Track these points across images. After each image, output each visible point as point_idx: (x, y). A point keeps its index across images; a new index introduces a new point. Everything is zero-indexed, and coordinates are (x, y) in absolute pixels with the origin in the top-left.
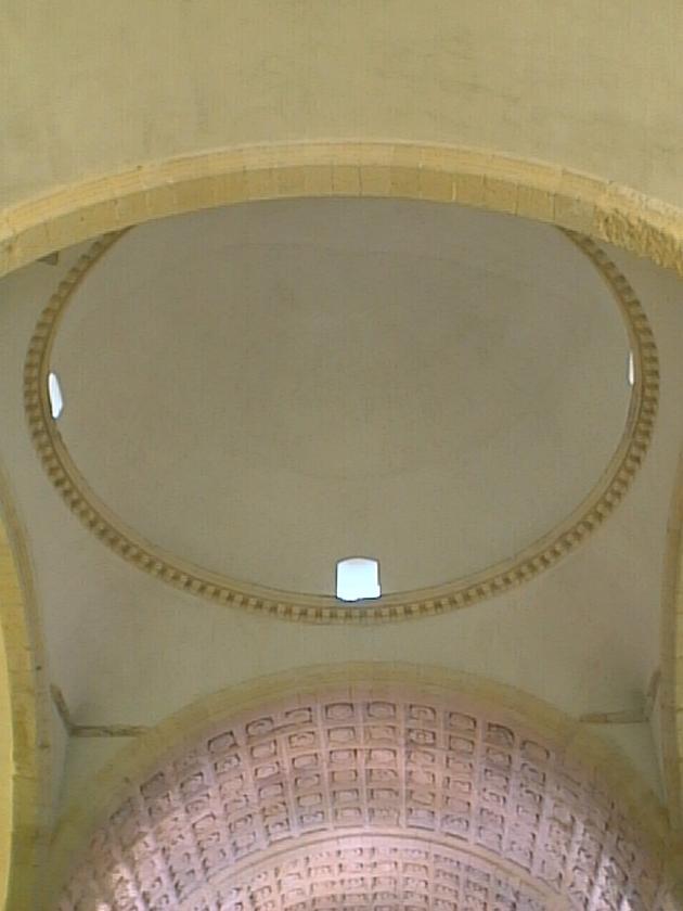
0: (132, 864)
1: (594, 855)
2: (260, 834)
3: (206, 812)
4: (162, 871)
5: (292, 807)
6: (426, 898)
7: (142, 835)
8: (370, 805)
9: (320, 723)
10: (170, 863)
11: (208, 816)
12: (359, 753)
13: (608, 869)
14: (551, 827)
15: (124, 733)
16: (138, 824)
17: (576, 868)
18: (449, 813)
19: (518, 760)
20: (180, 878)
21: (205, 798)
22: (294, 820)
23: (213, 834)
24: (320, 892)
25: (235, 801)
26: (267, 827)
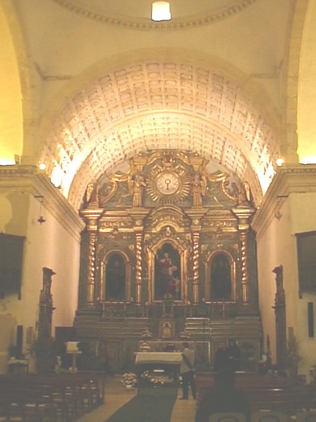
0: (70, 128)
1: (255, 127)
2: (122, 112)
3: (100, 105)
4: (82, 129)
5: (134, 102)
6: (190, 136)
8: (167, 101)
9: (145, 70)
10: (85, 125)
11: (100, 107)
12: (161, 82)
13: (260, 133)
14: (238, 115)
15: (65, 78)
16: (72, 113)
17: (248, 131)
18: (199, 105)
19: (225, 87)
20: (90, 131)
21: (99, 101)
22: (135, 107)
23: (102, 114)
24: (146, 133)
25: (111, 101)
26: (124, 110)
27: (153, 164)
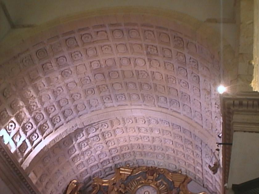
7: (39, 78)
15: (29, 26)
27: (138, 176)
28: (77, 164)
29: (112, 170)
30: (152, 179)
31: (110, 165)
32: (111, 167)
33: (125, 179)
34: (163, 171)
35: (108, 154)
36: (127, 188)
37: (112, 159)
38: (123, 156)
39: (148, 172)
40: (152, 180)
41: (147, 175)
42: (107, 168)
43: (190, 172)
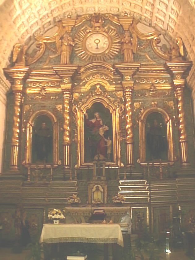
28: (18, 25)
29: (50, 24)
30: (99, 26)
31: (49, 20)
32: (50, 22)
33: (70, 32)
34: (107, 16)
35: (48, 8)
36: (75, 39)
37: (51, 13)
38: (62, 7)
39: (92, 19)
40: (99, 27)
41: (92, 22)
42: (45, 24)
43: (134, 12)
